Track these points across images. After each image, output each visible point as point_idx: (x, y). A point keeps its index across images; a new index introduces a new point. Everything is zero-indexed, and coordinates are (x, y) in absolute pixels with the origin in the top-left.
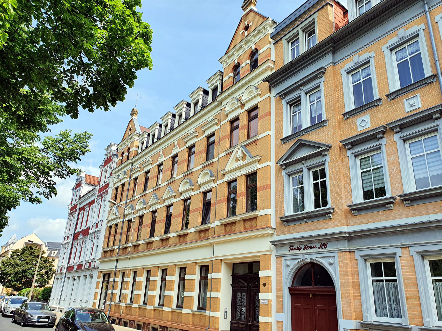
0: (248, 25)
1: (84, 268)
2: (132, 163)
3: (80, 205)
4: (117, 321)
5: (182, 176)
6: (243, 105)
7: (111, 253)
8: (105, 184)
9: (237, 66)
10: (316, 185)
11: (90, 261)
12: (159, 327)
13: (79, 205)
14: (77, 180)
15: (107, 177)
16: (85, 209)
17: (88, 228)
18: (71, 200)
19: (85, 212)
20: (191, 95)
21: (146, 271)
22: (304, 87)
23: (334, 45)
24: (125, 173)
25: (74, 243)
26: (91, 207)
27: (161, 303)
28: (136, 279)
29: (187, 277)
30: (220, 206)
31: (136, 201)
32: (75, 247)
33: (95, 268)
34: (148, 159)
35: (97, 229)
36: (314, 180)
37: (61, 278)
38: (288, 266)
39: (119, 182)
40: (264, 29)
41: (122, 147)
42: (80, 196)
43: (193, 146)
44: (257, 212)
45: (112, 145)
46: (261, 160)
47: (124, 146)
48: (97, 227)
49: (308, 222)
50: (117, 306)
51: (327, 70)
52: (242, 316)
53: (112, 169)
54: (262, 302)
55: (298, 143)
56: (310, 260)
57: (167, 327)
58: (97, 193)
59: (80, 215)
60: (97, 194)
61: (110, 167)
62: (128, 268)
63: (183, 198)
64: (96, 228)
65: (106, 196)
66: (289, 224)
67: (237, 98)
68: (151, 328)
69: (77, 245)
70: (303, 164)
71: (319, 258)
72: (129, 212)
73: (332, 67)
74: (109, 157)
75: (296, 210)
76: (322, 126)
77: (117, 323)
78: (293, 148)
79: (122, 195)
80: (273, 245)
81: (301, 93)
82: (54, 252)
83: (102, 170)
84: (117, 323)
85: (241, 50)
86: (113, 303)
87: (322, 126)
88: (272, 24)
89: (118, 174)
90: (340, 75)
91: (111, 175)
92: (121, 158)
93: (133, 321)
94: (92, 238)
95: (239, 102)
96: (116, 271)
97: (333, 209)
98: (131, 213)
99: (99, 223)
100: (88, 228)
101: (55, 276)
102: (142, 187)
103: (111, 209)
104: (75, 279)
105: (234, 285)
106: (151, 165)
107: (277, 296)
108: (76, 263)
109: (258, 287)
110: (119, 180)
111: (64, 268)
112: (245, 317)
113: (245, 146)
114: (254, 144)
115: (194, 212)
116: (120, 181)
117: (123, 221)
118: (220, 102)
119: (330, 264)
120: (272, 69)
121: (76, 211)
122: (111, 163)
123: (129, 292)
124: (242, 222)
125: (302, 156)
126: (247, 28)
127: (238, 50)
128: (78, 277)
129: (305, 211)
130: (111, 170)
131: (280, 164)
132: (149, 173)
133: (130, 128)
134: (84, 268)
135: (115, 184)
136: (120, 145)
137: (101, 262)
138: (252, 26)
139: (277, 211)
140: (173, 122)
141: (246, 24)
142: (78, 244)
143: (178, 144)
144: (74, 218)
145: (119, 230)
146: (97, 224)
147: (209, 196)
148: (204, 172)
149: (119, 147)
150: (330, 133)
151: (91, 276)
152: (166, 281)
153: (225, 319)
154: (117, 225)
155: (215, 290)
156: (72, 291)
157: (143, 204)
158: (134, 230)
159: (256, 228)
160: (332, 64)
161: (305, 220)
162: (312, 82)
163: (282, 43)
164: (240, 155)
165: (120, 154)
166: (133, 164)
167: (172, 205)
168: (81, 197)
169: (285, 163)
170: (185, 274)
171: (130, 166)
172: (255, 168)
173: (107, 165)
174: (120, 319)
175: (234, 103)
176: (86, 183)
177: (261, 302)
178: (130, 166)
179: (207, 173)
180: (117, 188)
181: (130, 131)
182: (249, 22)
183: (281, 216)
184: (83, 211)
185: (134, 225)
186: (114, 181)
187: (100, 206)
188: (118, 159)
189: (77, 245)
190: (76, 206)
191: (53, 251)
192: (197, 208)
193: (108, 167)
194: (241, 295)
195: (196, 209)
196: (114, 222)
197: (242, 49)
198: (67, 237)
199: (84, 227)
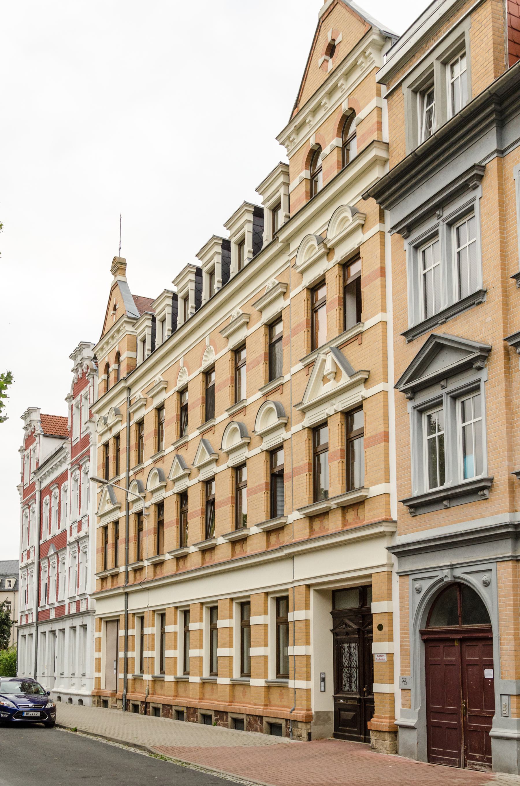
0: (334, 40)
1: (69, 613)
2: (129, 389)
3: (41, 483)
4: (141, 708)
5: (259, 394)
6: (330, 252)
7: (112, 582)
8: (82, 437)
9: (316, 151)
10: (432, 442)
11: (78, 598)
12: (213, 714)
13: (37, 483)
14: (25, 428)
15: (83, 422)
16: (52, 492)
17: (64, 532)
18: (21, 473)
19: (53, 498)
20: (228, 225)
21: (207, 609)
22: (444, 209)
23: (498, 108)
24: (117, 412)
25: (41, 563)
26: (62, 487)
27: (246, 671)
28: (188, 627)
29: (292, 616)
30: (300, 479)
31: (146, 472)
32: (46, 571)
33: (87, 613)
34: (157, 379)
35: (82, 534)
36: (429, 434)
37: (31, 635)
38: (419, 591)
39: (326, 258)
40: (366, 58)
41: (104, 352)
42: (37, 463)
43: (278, 319)
44: (364, 492)
45: (83, 346)
46: (288, 424)
47: (107, 349)
48: (79, 530)
49: (450, 507)
50: (137, 679)
51: (487, 169)
52: (353, 685)
53: (92, 402)
54: (378, 658)
55: (431, 342)
56: (453, 579)
57: (227, 713)
58: (69, 455)
59: (44, 505)
60: (69, 461)
61: (86, 398)
62: (147, 610)
63: (177, 492)
64: (78, 532)
65: (87, 464)
66: (420, 511)
67: (318, 234)
68: (199, 715)
69: (49, 568)
70: (443, 387)
71: (467, 573)
72: (135, 498)
73: (496, 159)
74: (80, 376)
75: (433, 484)
76: (476, 302)
77: (142, 711)
78: (422, 356)
79: (117, 459)
80: (393, 553)
81: (438, 225)
82: (10, 582)
83: (72, 405)
84: (142, 711)
85: (321, 113)
86: (130, 676)
87: (476, 302)
88: (382, 42)
89: (104, 413)
90: (513, 180)
91: (91, 415)
92: (104, 377)
93: (168, 705)
94: (74, 552)
95: (322, 244)
96: (127, 615)
97: (491, 480)
98: (138, 499)
99: (83, 521)
100: (64, 532)
101: (18, 630)
102: (262, 368)
103: (102, 491)
104: (55, 634)
105: (338, 630)
106: (360, 230)
107: (401, 646)
108: (53, 604)
109: (371, 631)
110: (107, 428)
111: (31, 615)
112: (358, 686)
113: (339, 348)
114: (356, 343)
115: (255, 494)
116: (110, 429)
117: (128, 517)
118: (286, 244)
119: (486, 584)
120: (385, 162)
121: (34, 497)
122: (87, 388)
123: (155, 654)
124: (340, 512)
125: (439, 373)
126: (331, 50)
127: (314, 112)
128: (60, 630)
129: (448, 484)
130: (89, 405)
131: (402, 389)
132: (187, 393)
133: (115, 306)
134: (69, 613)
135: (302, 273)
136: (100, 347)
137: (98, 599)
138: (341, 44)
139: (399, 487)
140: (258, 229)
141: (330, 40)
142: (49, 567)
143: (212, 342)
144: (34, 512)
145: (122, 535)
146: (80, 523)
147: (281, 456)
148: (230, 430)
149: (97, 352)
150: (489, 319)
151: (84, 627)
152: (249, 626)
153: (321, 691)
154: (116, 523)
155: (300, 641)
156: (55, 657)
157: (238, 435)
158: (295, 472)
159: (365, 522)
160: (495, 155)
161: (445, 503)
162: (420, 226)
163: (401, 94)
164: (329, 369)
165: (102, 368)
166: (130, 389)
167: (280, 447)
168: (40, 465)
169: (410, 387)
170: (287, 611)
171: (125, 395)
172: (357, 399)
173: (80, 394)
174: (146, 704)
175: (346, 217)
176: (46, 436)
177: (376, 658)
178: (125, 395)
179: (270, 410)
180: (106, 445)
181: (114, 312)
182: (335, 32)
183: (406, 497)
184: (48, 497)
185: (149, 524)
186: (98, 431)
187: (79, 484)
188: (100, 380)
189: (49, 568)
190: (32, 487)
191: (7, 580)
192: (258, 486)
193: (83, 399)
194: (349, 647)
195: (257, 487)
196: (110, 519)
197: (340, 90)
198: (26, 552)
199: (56, 531)
